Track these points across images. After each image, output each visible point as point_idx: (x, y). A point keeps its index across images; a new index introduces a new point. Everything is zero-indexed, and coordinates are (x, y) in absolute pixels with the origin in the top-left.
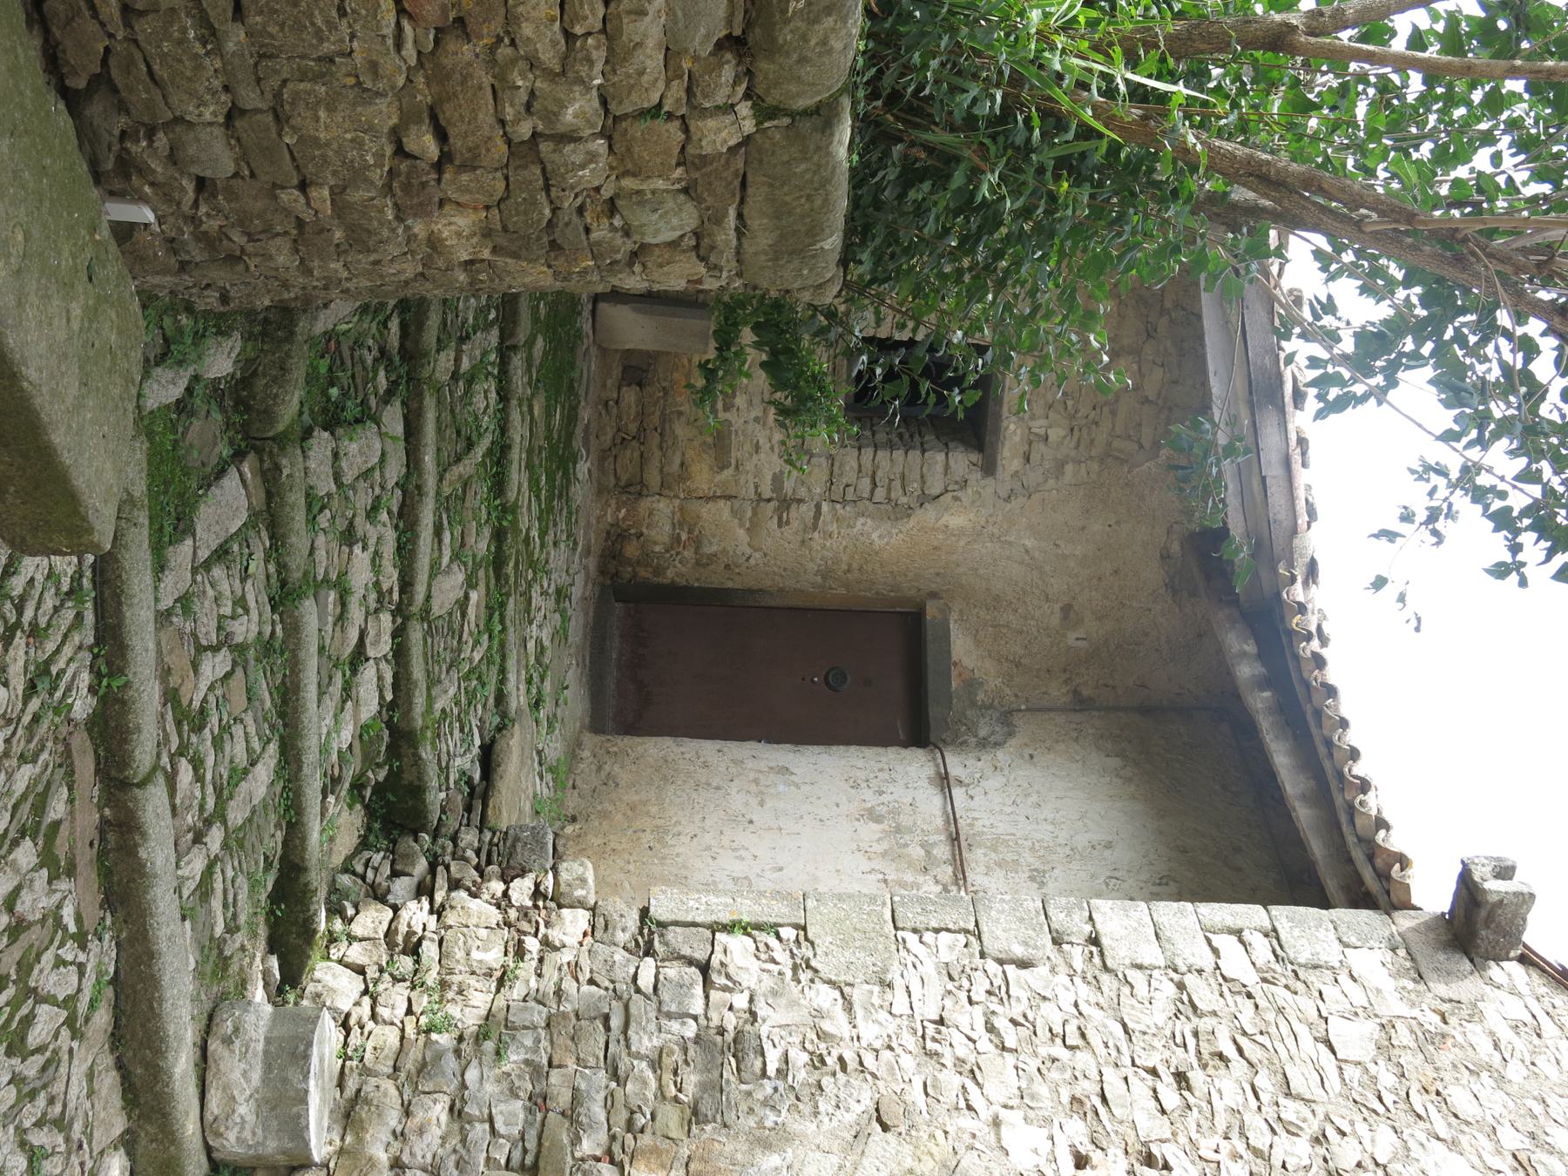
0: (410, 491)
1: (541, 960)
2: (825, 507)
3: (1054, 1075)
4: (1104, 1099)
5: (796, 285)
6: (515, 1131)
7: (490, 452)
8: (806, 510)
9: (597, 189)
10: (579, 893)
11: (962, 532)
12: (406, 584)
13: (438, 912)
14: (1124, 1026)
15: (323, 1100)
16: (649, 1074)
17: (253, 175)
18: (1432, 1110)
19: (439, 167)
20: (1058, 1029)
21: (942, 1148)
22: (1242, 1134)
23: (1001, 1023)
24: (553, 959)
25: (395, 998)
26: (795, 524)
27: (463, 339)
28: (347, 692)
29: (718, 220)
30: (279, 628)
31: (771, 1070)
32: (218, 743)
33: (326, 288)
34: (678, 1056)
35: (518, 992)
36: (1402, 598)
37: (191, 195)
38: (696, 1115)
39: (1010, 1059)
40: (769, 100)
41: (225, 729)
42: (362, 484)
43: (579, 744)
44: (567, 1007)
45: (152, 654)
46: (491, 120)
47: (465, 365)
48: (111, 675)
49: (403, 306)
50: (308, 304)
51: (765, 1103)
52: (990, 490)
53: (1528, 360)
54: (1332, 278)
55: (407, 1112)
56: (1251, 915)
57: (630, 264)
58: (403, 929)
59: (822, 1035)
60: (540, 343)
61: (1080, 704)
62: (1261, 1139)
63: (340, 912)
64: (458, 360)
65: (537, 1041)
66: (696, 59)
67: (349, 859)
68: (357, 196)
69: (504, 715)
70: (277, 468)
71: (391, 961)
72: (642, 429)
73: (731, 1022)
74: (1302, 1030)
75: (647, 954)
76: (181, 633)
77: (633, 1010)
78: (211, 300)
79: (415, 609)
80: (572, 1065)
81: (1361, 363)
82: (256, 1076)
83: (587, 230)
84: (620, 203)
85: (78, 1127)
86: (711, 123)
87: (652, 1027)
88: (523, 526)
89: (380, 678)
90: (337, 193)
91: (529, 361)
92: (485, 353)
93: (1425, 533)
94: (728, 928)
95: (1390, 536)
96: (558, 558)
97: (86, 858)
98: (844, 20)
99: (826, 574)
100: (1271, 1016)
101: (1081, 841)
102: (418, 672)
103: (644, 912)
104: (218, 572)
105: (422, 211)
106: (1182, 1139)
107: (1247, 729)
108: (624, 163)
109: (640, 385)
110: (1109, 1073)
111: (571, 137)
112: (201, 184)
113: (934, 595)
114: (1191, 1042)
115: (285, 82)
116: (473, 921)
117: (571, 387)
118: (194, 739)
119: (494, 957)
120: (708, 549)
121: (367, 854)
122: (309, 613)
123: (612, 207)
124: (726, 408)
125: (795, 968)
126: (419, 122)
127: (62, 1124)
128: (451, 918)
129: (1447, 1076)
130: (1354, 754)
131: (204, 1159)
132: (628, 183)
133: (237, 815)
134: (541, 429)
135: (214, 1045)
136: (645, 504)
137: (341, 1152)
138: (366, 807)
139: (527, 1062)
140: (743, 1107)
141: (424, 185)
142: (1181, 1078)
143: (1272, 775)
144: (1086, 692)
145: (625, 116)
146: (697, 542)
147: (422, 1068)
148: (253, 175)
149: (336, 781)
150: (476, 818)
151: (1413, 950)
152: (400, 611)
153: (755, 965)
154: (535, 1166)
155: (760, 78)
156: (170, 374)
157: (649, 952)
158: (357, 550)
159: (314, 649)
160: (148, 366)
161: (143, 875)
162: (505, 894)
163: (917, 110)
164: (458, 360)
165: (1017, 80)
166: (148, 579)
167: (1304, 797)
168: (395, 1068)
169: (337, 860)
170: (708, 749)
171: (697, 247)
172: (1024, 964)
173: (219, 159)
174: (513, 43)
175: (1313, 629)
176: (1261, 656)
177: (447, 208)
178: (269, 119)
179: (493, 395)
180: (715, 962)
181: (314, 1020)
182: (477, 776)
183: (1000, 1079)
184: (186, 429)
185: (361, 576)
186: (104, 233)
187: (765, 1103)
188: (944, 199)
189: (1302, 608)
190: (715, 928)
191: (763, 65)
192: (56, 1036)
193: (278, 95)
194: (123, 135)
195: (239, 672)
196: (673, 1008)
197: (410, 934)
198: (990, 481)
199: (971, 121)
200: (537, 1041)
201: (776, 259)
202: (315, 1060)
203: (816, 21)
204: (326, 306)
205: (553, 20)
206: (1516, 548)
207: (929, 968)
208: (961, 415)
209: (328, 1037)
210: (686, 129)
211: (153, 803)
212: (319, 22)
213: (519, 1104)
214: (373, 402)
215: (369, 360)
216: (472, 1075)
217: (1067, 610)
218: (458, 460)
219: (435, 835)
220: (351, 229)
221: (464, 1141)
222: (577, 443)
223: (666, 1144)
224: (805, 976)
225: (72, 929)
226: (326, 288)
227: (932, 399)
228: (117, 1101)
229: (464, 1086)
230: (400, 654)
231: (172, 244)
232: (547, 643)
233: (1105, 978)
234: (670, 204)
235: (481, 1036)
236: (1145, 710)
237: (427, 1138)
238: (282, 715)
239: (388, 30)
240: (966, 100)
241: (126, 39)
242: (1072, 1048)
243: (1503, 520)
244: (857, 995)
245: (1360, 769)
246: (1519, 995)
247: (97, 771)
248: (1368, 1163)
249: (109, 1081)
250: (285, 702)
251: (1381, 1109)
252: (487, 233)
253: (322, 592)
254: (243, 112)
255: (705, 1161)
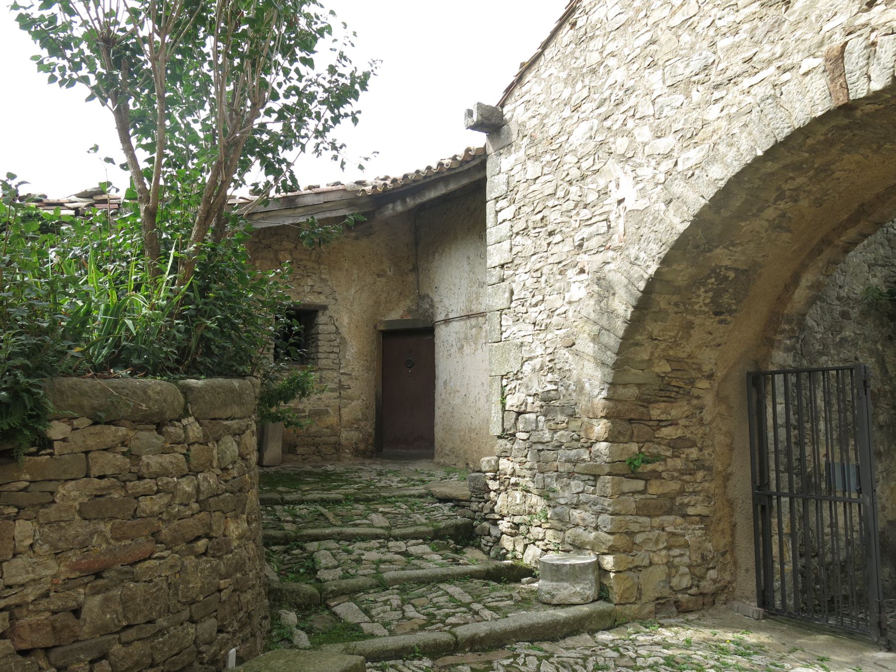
0: (340, 537)
1: (519, 476)
2: (342, 371)
3: (552, 281)
4: (560, 263)
5: (253, 394)
6: (582, 484)
7: (324, 506)
8: (344, 378)
9: (218, 475)
10: (493, 463)
11: (350, 317)
12: (377, 537)
13: (503, 517)
14: (533, 255)
15: (573, 558)
16: (558, 433)
17: (216, 611)
18: (558, 141)
19: (210, 538)
20: (535, 280)
21: (580, 323)
22: (570, 211)
23: (534, 301)
24: (518, 472)
25: (536, 532)
26: (349, 383)
27: (280, 520)
28: (419, 558)
29: (228, 428)
30: (395, 587)
31: (555, 387)
32: (440, 608)
33: (260, 578)
34: (552, 423)
35: (531, 485)
36: (367, 159)
37: (224, 635)
38: (572, 416)
39: (547, 298)
40: (181, 412)
41: (434, 605)
42: (338, 557)
43: (438, 463)
44: (536, 466)
45: (406, 636)
46: (191, 520)
47: (289, 518)
48: (414, 652)
49: (266, 545)
50: (267, 584)
51: (567, 390)
52: (333, 307)
53: (274, 112)
54: (244, 182)
55: (577, 525)
56: (490, 207)
57: (247, 460)
58: (509, 530)
59: (541, 368)
60: (280, 489)
61: (415, 269)
62: (571, 205)
63: (505, 554)
64: (288, 522)
65: (548, 477)
66: (165, 442)
67: (484, 553)
68: (223, 569)
69: (427, 495)
70: (332, 591)
71: (522, 534)
72: (313, 445)
73: (538, 403)
74: (532, 188)
75: (515, 436)
76: (397, 626)
77: (536, 440)
78: (266, 623)
79: (386, 533)
80: (556, 464)
81: (278, 173)
82: (565, 584)
83: (234, 478)
84: (223, 466)
85: (586, 652)
86: (191, 434)
87: (541, 433)
88: (352, 491)
89: (414, 545)
90: (222, 577)
91: (287, 492)
92: (285, 511)
93: (341, 151)
94: (504, 405)
95: (343, 163)
96: (366, 476)
97: (485, 657)
98: (149, 386)
99: (368, 369)
100: (527, 200)
101: (467, 268)
102: (411, 530)
103: (499, 437)
104: (373, 612)
105: (228, 543)
106: (573, 233)
107: (422, 207)
108: (207, 466)
109: (296, 447)
110: (550, 260)
111: (198, 489)
112: (220, 631)
113: (375, 327)
114: (537, 230)
115: (179, 601)
116: (505, 503)
117: (297, 474)
118: (438, 617)
119: (518, 495)
120: (360, 416)
121: (482, 546)
122: (387, 575)
123: (224, 469)
124: (304, 412)
125: (517, 379)
126: (193, 547)
127: (585, 659)
128: (505, 512)
129: (546, 135)
130: (429, 168)
131: (598, 603)
132: (215, 464)
133: (467, 598)
134: (314, 486)
135: (555, 602)
136: (343, 442)
137: (593, 550)
138: (464, 547)
139: (556, 480)
140: (569, 398)
141: (218, 543)
142: (551, 234)
143: (439, 198)
144: (411, 267)
145: (189, 467)
146: (358, 420)
147: (560, 520)
148: (216, 611)
149: (454, 560)
150: (467, 504)
151: (500, 147)
152: (388, 538)
153: (517, 394)
154: (594, 475)
155: (172, 417)
156: (296, 638)
157: (514, 435)
158: (363, 557)
159: (403, 572)
160: (293, 646)
161: (491, 634)
162: (495, 491)
163: (184, 352)
164: (288, 522)
165: (171, 315)
166: (376, 640)
167: (446, 186)
168: (561, 531)
169: (485, 557)
170: (438, 413)
171: (239, 435)
172: (512, 293)
173: (210, 624)
174: (161, 513)
175: (382, 182)
176: (394, 202)
177: (227, 533)
178: (193, 606)
179: (301, 506)
180: (516, 410)
181: (544, 563)
182: (451, 504)
183: (555, 301)
184: (318, 629)
185: (374, 555)
186: (241, 668)
187: (567, 390)
188: (219, 340)
189: (374, 187)
190: (504, 410)
191: (168, 415)
192: (552, 663)
193: (184, 604)
194: (201, 663)
195: (412, 601)
196: (534, 425)
197: (511, 527)
198: (329, 307)
199: (187, 331)
200: (548, 477)
201: (243, 404)
202: (559, 562)
203: (149, 397)
204: (267, 577)
205: (152, 499)
206: (346, 115)
207: (515, 329)
208: (302, 326)
209: (552, 558)
210: (194, 443)
211: (463, 632)
212: (154, 590)
213: (572, 483)
214: (305, 555)
215: (289, 557)
216: (562, 501)
217: (379, 276)
218: (327, 519)
219: (474, 519)
220: (236, 571)
221: (586, 503)
222: (320, 470)
223: (584, 426)
224: (520, 376)
225: (512, 660)
226: (260, 578)
227: (296, 337)
228: (577, 638)
229: (566, 504)
230: (404, 538)
231: (244, 641)
232: (399, 479)
233: (516, 262)
234: (223, 447)
235: (547, 498)
236: (417, 244)
237: (586, 517)
238: (429, 583)
239: (157, 562)
240: (178, 335)
241: (163, 665)
242: (542, 274)
243: (336, 120)
244: (526, 356)
245: (434, 166)
246: (515, 108)
247: (452, 655)
248: (578, 165)
249: (569, 642)
250: (424, 582)
251: (558, 160)
252: (236, 517)
253: (381, 570)
254: (191, 617)
255: (588, 412)
